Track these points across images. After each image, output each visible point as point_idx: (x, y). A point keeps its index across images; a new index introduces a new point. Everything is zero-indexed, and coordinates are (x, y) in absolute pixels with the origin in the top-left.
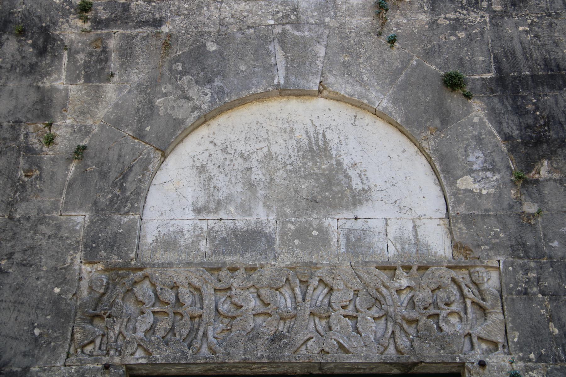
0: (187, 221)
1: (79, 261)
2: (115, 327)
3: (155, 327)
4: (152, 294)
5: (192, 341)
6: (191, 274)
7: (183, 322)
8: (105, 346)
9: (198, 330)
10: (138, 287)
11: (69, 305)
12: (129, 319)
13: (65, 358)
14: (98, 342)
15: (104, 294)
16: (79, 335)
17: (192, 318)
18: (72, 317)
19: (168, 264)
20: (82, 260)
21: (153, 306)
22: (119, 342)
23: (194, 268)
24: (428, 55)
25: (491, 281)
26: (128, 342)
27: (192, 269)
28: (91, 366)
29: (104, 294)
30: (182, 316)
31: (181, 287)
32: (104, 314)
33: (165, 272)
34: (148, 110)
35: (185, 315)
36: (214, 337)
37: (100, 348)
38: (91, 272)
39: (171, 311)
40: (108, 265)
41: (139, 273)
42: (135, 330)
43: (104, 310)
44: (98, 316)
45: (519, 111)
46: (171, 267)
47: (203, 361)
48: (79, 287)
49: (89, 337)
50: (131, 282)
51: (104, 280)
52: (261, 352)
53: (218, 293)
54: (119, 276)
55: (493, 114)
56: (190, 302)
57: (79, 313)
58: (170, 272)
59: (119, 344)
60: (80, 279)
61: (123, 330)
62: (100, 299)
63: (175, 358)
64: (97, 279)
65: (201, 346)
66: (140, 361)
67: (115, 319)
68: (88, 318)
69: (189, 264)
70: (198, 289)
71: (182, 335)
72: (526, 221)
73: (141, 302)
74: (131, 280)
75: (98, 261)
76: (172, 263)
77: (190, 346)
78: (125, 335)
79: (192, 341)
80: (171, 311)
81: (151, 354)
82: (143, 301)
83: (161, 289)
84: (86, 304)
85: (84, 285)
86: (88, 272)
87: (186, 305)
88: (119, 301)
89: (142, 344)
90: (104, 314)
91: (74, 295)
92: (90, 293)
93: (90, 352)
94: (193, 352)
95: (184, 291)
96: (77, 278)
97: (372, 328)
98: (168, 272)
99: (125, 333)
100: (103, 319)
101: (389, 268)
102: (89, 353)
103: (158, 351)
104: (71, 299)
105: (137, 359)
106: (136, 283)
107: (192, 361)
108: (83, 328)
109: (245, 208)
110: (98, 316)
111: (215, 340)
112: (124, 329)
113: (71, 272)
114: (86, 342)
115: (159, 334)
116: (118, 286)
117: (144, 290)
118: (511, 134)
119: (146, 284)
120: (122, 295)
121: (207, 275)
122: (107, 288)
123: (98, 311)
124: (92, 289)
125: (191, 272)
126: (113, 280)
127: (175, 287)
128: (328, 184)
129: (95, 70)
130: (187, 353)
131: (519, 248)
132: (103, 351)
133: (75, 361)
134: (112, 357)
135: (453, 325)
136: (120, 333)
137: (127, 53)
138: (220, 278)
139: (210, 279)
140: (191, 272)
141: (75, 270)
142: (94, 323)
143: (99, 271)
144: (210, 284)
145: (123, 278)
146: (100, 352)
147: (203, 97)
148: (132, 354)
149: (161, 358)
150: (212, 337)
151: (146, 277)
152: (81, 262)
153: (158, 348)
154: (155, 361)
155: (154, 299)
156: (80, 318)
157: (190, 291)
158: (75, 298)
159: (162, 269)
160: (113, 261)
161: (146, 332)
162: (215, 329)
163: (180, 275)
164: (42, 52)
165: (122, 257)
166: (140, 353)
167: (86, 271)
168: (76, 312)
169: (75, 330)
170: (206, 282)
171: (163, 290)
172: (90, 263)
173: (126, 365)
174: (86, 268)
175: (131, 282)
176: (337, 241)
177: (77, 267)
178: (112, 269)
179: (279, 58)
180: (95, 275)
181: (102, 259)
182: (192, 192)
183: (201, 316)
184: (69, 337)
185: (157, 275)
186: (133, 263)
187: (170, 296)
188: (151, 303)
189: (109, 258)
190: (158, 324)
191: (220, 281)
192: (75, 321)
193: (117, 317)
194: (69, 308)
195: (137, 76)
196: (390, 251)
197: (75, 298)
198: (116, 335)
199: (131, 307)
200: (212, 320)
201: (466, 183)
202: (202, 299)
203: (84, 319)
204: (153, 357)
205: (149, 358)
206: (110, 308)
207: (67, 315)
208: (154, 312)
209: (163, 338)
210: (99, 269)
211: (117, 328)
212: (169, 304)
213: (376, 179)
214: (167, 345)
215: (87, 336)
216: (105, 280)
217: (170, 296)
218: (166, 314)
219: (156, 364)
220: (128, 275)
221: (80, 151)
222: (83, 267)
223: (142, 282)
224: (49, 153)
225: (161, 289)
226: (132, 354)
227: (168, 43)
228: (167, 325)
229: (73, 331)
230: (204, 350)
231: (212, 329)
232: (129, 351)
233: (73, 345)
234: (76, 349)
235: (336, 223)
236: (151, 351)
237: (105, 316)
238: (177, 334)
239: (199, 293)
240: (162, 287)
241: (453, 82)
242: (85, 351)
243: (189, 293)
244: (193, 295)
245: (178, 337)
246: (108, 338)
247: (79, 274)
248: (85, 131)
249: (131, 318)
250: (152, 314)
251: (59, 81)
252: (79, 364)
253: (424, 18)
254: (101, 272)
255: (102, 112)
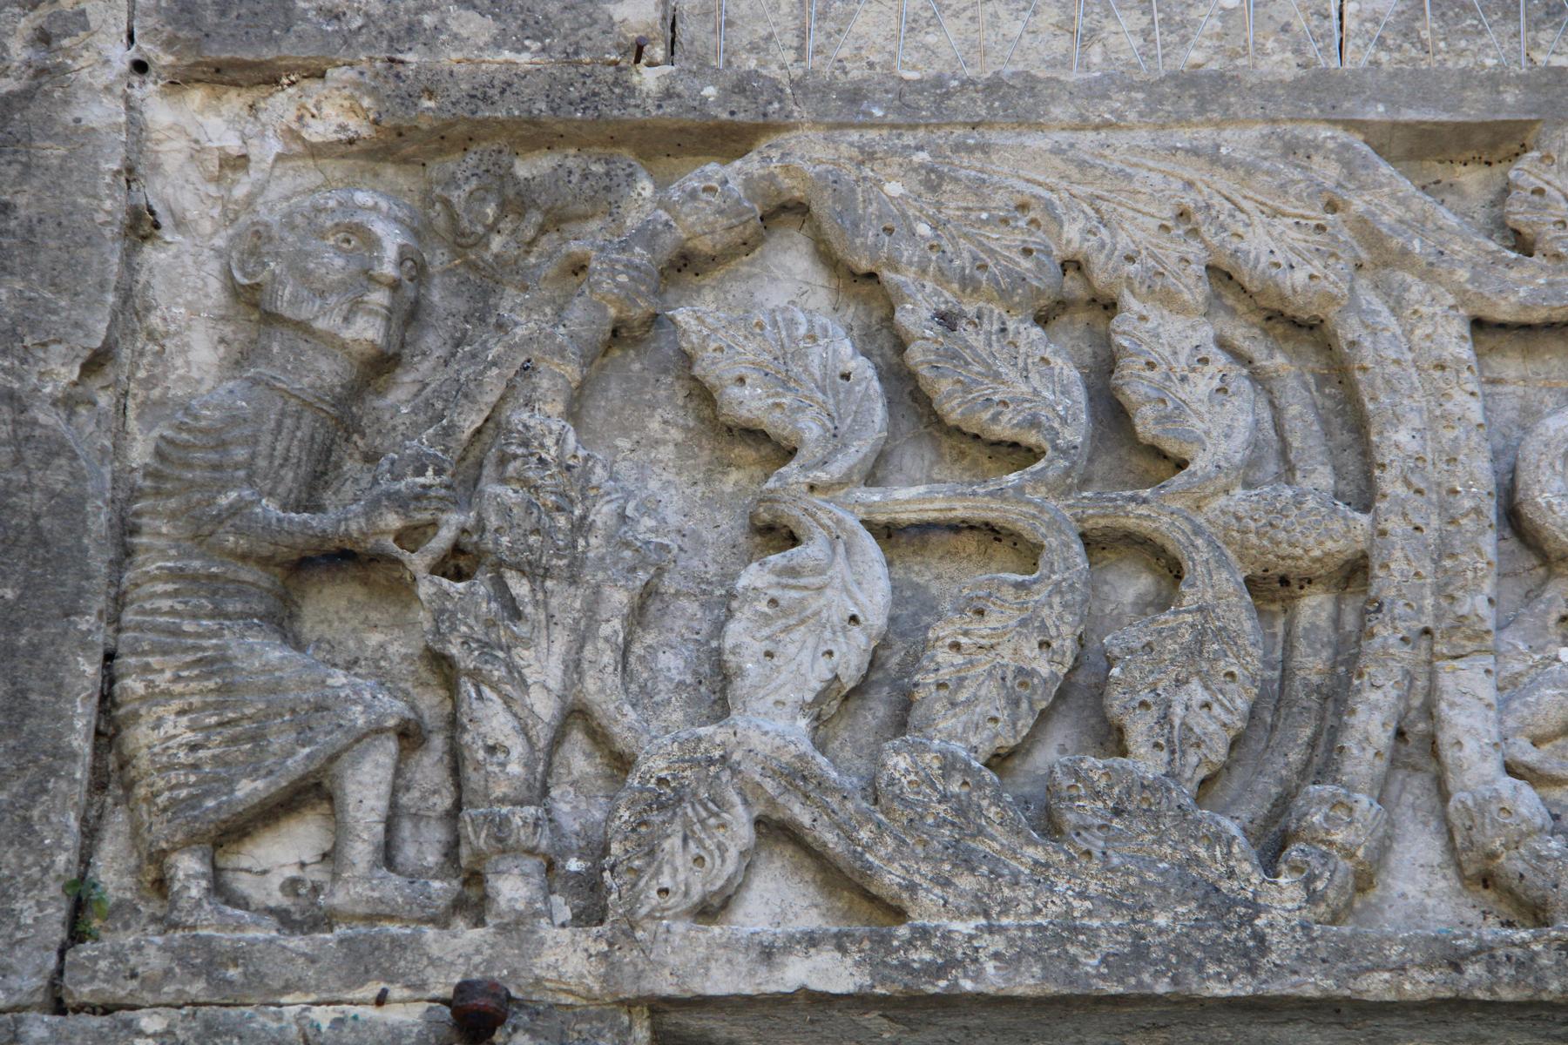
1: (121, 57)
2: (523, 656)
3: (913, 662)
4: (863, 368)
5: (1283, 803)
6: (1224, 181)
7: (1181, 620)
8: (436, 834)
9: (1336, 697)
10: (707, 303)
11: (55, 449)
12: (649, 592)
13: (59, 934)
14: (366, 786)
15: (381, 366)
16: (178, 729)
17: (1272, 588)
18: (99, 562)
19: (993, 87)
20: (147, 48)
21: (875, 473)
22: (564, 803)
23: (1256, 131)
26: (667, 799)
27: (1239, 141)
28: (323, 1016)
29: (381, 366)
30: (1173, 571)
31: (1132, 304)
32: (412, 537)
33: (967, 166)
35: (1198, 559)
36: (1510, 769)
37: (387, 855)
38: (240, 162)
39: (1055, 525)
40: (409, 100)
41: (712, 168)
42: (717, 687)
43: (401, 503)
44: (344, 560)
46: (1029, 122)
47: (1420, 985)
48: (131, 304)
49: (277, 743)
50: (640, 254)
51: (379, 228)
53: (1510, 366)
54: (517, 201)
56: (1241, 436)
57: (160, 543)
58: (1021, 161)
59: (571, 825)
60: (142, 226)
61: (601, 688)
62: (342, 418)
63: (1139, 951)
64: (310, 223)
65: (1383, 848)
66: (796, 973)
67: (520, 587)
68: (249, 574)
69: (1205, 92)
70: (1300, 327)
71: (1192, 738)
73: (753, 434)
74: (647, 235)
75: (309, 53)
76: (1030, 84)
77: (1274, 844)
78: (623, 737)
79: (1283, 803)
80: (1055, 525)
81: (900, 914)
82: (773, 422)
83: (947, 320)
84: (222, 445)
85: (185, 282)
87: (1201, 463)
88: (544, 418)
89: (802, 814)
90: (412, 537)
91: (96, 363)
92: (240, 361)
93: (292, 886)
94: (1313, 898)
95: (1170, 341)
96: (111, 206)
98: (1001, 167)
99: (624, 722)
100: (401, 589)
102: (277, 899)
103: (966, 882)
104: (68, 403)
105: (768, 954)
106: (685, 265)
107: (1314, 983)
108: (211, 665)
110: (344, 560)
111: (1527, 791)
112: (613, 680)
113: (53, 152)
114: (249, 789)
115: (963, 725)
116: (509, 301)
117: (773, 326)
118: (1166, 312)
119: (789, 278)
120: (572, 372)
121: (1390, 194)
122: (410, 315)
123: (344, 515)
124: (271, 319)
125: (1229, 165)
126: (462, 241)
127: (1078, 303)
130: (1255, 908)
132: (415, 875)
133: (154, 961)
134: (517, 927)
136: (576, 715)
138: (1519, 213)
139: (1420, 225)
140: (1229, 165)
141: (80, 136)
142: (310, 623)
143: (316, 151)
144: (1428, 274)
145: (557, 220)
146: (392, 887)
148: (710, 910)
149: (998, 943)
150: (1492, 767)
151: (783, 211)
152: (140, 67)
153: (967, 862)
154: (939, 971)
155: (879, 412)
156: (175, 575)
157: (1222, 344)
158: (104, 400)
159: (939, 136)
160: (450, 58)
161: (834, 705)
162: (1509, 688)
163: (1127, 201)
165: (539, 29)
166: (778, 900)
167: (197, 152)
168: (126, 530)
169: (134, 685)
170: (1380, 255)
171: (966, 332)
172: (220, 75)
173: (658, 1006)
174: (193, 126)
175: (640, 254)
177: (101, 113)
178: (449, 138)
180: (281, 191)
181: (348, 39)
183: (1354, 573)
184: (80, 741)
185: (894, 188)
186: (648, 79)
187: (1038, 382)
188: (859, 451)
189: (412, 30)
190: (943, 631)
191: (1523, 244)
192: (119, 601)
193: (536, 572)
194: (57, 478)
197: (104, 400)
198: (542, 736)
199: (656, 485)
200: (1476, 604)
202: (1352, 424)
203: (212, 585)
204: (924, 934)
205: (883, 941)
206: (466, 487)
207: (40, 540)
208: (887, 533)
209: (1000, 761)
210: (318, 132)
211: (544, 667)
212: (1031, 454)
214: (1050, 826)
215: (256, 737)
216: (391, 239)
217: (1038, 382)
218: (1002, 551)
219: (950, 1002)
220: (605, 197)
222: (160, 112)
223: (742, 265)
225: (947, 320)
226: (710, 910)
228: (1030, 649)
229: (107, 700)
230: (1419, 889)
231: (1487, 691)
232: (679, 873)
233: (118, 821)
234: (158, 858)
236: (890, 878)
237: (418, 562)
238: (1139, 730)
239: (1315, 362)
240: (947, 298)
242: (244, 884)
243: (1220, 360)
244: (1258, 378)
245: (1146, 762)
246: (456, 763)
247: (130, 173)
249: (669, 585)
250: (869, 545)
252: (197, 988)
254: (335, 169)
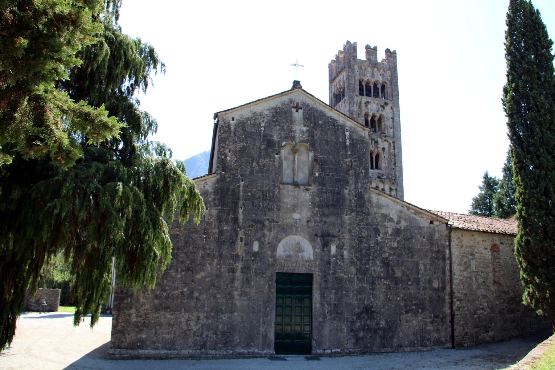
0: (282, 253)
24: (313, 230)
25: (317, 263)
34: (277, 237)
45: (324, 240)
52: (291, 272)
55: (321, 240)
72: (322, 256)
86: (271, 260)
97: (304, 269)
101: (306, 261)
109: (289, 252)
128: (300, 249)
129: (270, 230)
131: (321, 260)
135: (313, 269)
137: (274, 227)
147: (284, 235)
163: (282, 261)
164: (263, 226)
176: (300, 257)
179: (294, 229)
182: (282, 249)
195: (276, 231)
196: (306, 258)
201: (316, 250)
202: (501, 284)
213: (305, 249)
221: (269, 243)
224: (265, 243)
227: (280, 225)
235: (300, 254)
241: (316, 235)
248: (269, 240)
251: (265, 231)
253: (313, 224)
255: (271, 237)
